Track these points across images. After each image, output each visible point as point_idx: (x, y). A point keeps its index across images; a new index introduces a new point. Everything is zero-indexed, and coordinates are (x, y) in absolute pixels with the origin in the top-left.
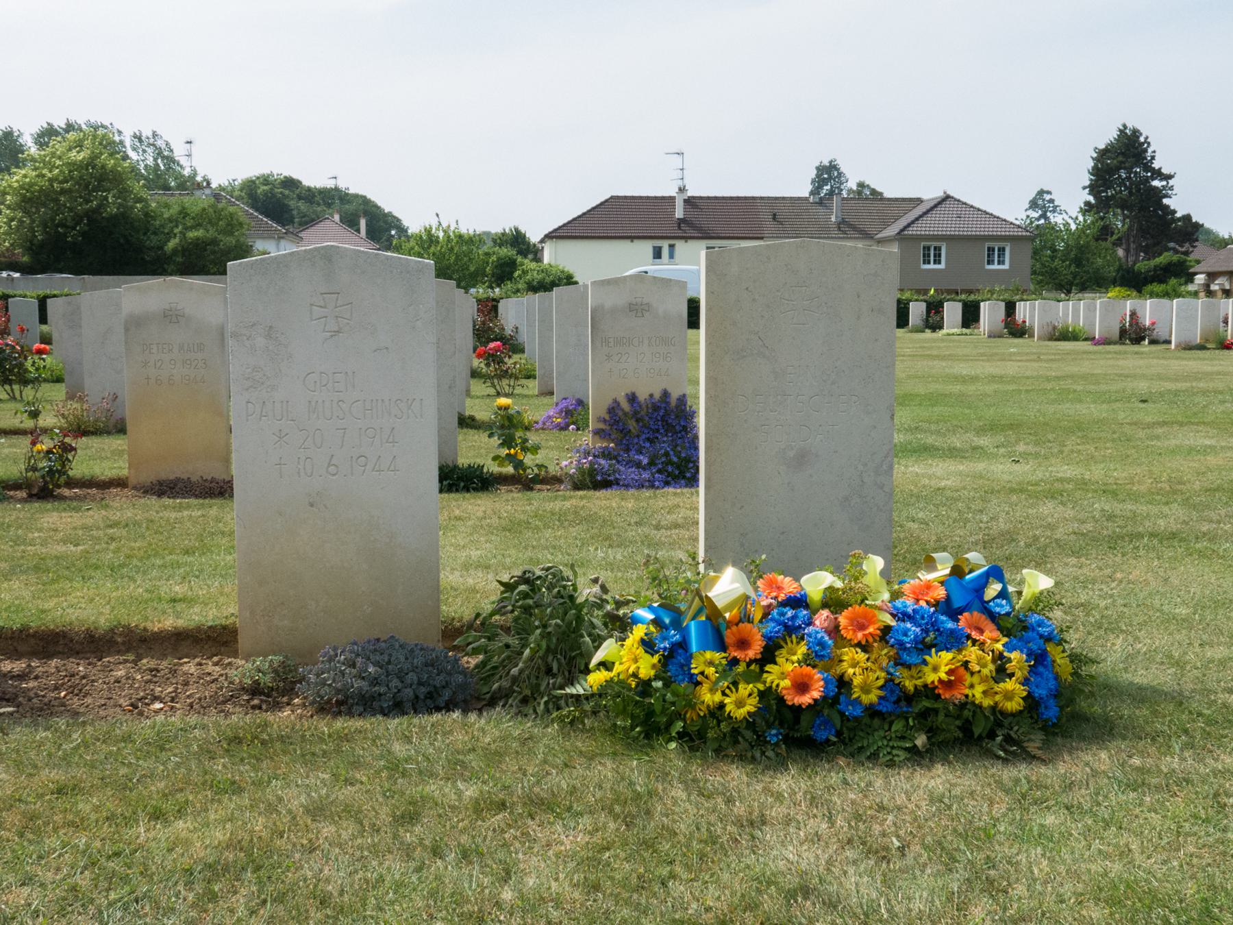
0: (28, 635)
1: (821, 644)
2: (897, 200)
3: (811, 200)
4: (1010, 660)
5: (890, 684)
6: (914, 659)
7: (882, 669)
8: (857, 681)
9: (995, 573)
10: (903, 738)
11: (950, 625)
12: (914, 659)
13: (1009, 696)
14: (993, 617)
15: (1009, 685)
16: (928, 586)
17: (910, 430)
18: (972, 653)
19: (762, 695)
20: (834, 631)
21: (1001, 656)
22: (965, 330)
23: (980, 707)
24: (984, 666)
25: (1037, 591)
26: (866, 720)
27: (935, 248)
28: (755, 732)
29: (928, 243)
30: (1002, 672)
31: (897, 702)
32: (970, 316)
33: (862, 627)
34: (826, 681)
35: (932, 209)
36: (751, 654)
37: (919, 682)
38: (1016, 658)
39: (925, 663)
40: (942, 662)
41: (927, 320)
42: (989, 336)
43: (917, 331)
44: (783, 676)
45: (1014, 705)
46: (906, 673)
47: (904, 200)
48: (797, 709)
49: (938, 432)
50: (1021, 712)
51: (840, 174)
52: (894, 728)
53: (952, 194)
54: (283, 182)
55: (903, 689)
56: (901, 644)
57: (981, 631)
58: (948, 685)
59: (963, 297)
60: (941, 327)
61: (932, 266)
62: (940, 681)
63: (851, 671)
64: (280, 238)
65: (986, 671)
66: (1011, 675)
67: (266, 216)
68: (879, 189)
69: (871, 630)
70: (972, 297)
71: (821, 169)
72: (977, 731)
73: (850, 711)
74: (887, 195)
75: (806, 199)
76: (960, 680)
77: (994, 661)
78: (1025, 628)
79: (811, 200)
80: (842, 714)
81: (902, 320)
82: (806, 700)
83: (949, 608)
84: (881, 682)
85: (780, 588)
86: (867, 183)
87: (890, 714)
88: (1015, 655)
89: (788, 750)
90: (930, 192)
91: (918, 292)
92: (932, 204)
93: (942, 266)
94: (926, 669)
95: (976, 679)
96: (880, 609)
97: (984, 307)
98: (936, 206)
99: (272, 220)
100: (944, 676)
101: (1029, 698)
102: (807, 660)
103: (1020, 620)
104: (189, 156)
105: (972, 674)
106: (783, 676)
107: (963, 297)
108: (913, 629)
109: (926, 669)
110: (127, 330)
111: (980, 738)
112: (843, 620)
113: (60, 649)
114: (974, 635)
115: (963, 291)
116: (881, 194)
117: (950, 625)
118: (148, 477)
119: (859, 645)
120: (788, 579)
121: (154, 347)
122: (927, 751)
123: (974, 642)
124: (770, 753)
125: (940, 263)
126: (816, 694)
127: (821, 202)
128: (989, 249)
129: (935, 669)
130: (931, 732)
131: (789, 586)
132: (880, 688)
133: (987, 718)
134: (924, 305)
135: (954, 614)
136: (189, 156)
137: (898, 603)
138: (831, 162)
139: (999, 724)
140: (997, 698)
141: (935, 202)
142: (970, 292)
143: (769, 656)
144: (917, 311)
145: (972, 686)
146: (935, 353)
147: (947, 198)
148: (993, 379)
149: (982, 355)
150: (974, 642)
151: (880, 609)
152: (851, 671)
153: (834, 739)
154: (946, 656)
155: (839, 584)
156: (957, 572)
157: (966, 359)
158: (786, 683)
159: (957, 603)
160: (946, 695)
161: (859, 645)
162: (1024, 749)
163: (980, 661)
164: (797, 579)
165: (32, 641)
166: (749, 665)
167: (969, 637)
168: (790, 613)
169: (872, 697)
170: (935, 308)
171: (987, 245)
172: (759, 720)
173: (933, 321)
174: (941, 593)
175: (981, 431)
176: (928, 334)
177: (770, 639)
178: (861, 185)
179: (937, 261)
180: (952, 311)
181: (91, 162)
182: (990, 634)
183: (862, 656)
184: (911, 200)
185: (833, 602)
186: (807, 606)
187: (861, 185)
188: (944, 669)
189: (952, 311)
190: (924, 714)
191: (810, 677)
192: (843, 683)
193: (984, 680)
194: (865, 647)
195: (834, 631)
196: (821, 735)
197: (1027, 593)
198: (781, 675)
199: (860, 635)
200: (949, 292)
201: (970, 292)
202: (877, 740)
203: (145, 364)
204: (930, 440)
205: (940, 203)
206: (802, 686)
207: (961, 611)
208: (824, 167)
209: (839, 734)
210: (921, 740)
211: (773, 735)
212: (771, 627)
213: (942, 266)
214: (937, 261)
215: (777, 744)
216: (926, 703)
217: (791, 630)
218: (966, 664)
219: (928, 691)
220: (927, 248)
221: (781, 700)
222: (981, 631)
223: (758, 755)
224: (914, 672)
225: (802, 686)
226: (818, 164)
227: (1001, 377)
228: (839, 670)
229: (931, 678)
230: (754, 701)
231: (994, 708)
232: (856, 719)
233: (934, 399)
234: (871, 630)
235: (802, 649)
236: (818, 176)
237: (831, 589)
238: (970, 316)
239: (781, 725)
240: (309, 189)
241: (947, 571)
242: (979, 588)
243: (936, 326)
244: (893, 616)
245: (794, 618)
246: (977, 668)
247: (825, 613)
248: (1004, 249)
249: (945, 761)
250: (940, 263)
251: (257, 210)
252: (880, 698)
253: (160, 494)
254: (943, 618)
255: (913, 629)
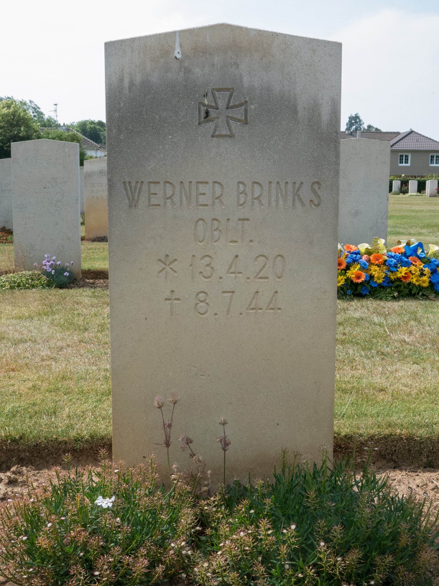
0: (91, 272)
1: (365, 264)
2: (387, 133)
3: (347, 132)
4: (425, 271)
5: (386, 277)
6: (394, 270)
7: (384, 273)
8: (376, 276)
9: (420, 245)
10: (390, 293)
11: (406, 260)
12: (394, 270)
13: (424, 282)
14: (420, 258)
15: (424, 278)
16: (399, 249)
17: (392, 227)
18: (412, 268)
19: (346, 280)
20: (369, 261)
21: (422, 270)
22: (419, 194)
23: (415, 285)
24: (417, 272)
25: (434, 251)
26: (378, 288)
27: (406, 156)
28: (343, 291)
29: (402, 154)
30: (422, 274)
31: (388, 283)
32: (421, 187)
33: (378, 260)
34: (366, 276)
35: (404, 137)
36: (342, 267)
37: (395, 277)
38: (427, 270)
39: (398, 271)
40: (403, 271)
41: (401, 189)
42: (430, 196)
43: (396, 194)
44: (352, 274)
45: (426, 285)
46: (391, 274)
47: (391, 133)
48: (357, 284)
49: (404, 228)
50: (428, 287)
51: (360, 121)
52: (387, 291)
53: (414, 130)
54: (98, 123)
55: (389, 278)
56: (390, 265)
57: (416, 262)
58: (405, 278)
59: (418, 178)
60: (407, 192)
61: (404, 164)
62: (402, 276)
63: (374, 273)
64: (97, 150)
65: (417, 274)
66: (425, 275)
67: (91, 139)
68: (379, 128)
69: (381, 260)
70: (422, 179)
71: (351, 118)
72: (413, 292)
73: (373, 285)
74: (384, 130)
75: (344, 132)
76: (409, 277)
77: (420, 271)
78: (430, 262)
79: (347, 132)
80: (371, 286)
81: (391, 190)
82: (360, 281)
83: (405, 254)
84: (383, 276)
85: (351, 249)
86: (372, 125)
87: (386, 287)
88: (426, 269)
89: (354, 297)
90: (403, 129)
91: (397, 176)
92: (404, 135)
93: (409, 165)
94: (398, 273)
95: (414, 276)
96: (384, 255)
97: (428, 183)
98: (406, 136)
99: (94, 141)
100: (403, 274)
101: (430, 282)
102: (360, 269)
103: (428, 259)
104: (56, 111)
105: (413, 274)
106: (352, 274)
107: (418, 178)
108: (394, 261)
109: (398, 273)
110: (85, 178)
111: (415, 294)
112: (371, 257)
113: (101, 277)
114: (414, 263)
115: (418, 176)
116: (380, 130)
117: (406, 260)
118: (92, 236)
119: (376, 265)
120: (354, 246)
121: (96, 185)
122: (398, 297)
123: (414, 265)
124: (348, 297)
125: (407, 163)
126: (363, 279)
127: (351, 134)
128: (431, 156)
129: (401, 273)
130: (399, 292)
131: (354, 248)
132: (383, 278)
133: (417, 288)
134: (400, 182)
135: (407, 257)
136: (56, 111)
137: (389, 253)
138: (356, 115)
139: (420, 290)
140: (420, 282)
141: (406, 134)
142: (422, 177)
143: (348, 268)
144: (397, 184)
145: (412, 278)
146: (404, 202)
147: (412, 132)
148: (430, 211)
149: (426, 203)
150: (414, 265)
151: (384, 255)
152: (374, 273)
153: (368, 294)
154: (404, 269)
155: (370, 248)
156: (408, 244)
157: (418, 204)
158: (354, 276)
159: (408, 254)
160: (404, 281)
161: (376, 265)
162: (428, 298)
163: (415, 270)
164: (356, 246)
165: (92, 274)
166: (342, 271)
167: (412, 264)
168: (354, 256)
169: (381, 281)
170: (405, 183)
171: (431, 154)
172: (344, 288)
173: (404, 189)
174: (403, 250)
175: (423, 227)
176: (401, 195)
177: (348, 263)
178: (369, 127)
179: (406, 162)
180: (413, 185)
181: (14, 114)
182: (418, 263)
183: (378, 268)
184: (394, 133)
185: (369, 253)
186: (360, 254)
187: (369, 127)
188: (404, 272)
189: (413, 185)
190: (398, 286)
191: (361, 274)
192: (372, 277)
193: (416, 276)
194: (378, 266)
195: (369, 261)
196: (364, 293)
197: (430, 252)
198: (352, 273)
199: (377, 262)
200: (412, 177)
201: (422, 177)
202: (382, 294)
203: (92, 191)
204: (401, 230)
205: (408, 134)
206: (358, 277)
207: (409, 256)
208: (353, 117)
209: (370, 292)
210: (396, 294)
211: (349, 292)
212: (348, 260)
213: (409, 165)
214: (406, 162)
215: (350, 295)
216: (398, 283)
217: (355, 261)
218: (410, 271)
219: (399, 279)
220: (401, 156)
221: (352, 282)
222: (416, 262)
223: (344, 298)
224: (394, 274)
225: (358, 277)
226: (349, 116)
227: (434, 211)
228: (370, 272)
229: (399, 275)
230: (344, 280)
231: (419, 285)
232: (375, 287)
233: (403, 217)
234: (381, 260)
235: (359, 266)
236: (349, 121)
237: (367, 249)
238: (421, 187)
239: (352, 289)
240: (68, 128)
241: (405, 244)
242: (415, 250)
243: (405, 192)
244: (388, 257)
245: (355, 257)
246: (414, 272)
247: (366, 256)
248: (408, 157)
249: (403, 300)
250: (407, 163)
251: (86, 137)
252: (383, 281)
253: (99, 241)
254: (404, 258)
255: (394, 261)
